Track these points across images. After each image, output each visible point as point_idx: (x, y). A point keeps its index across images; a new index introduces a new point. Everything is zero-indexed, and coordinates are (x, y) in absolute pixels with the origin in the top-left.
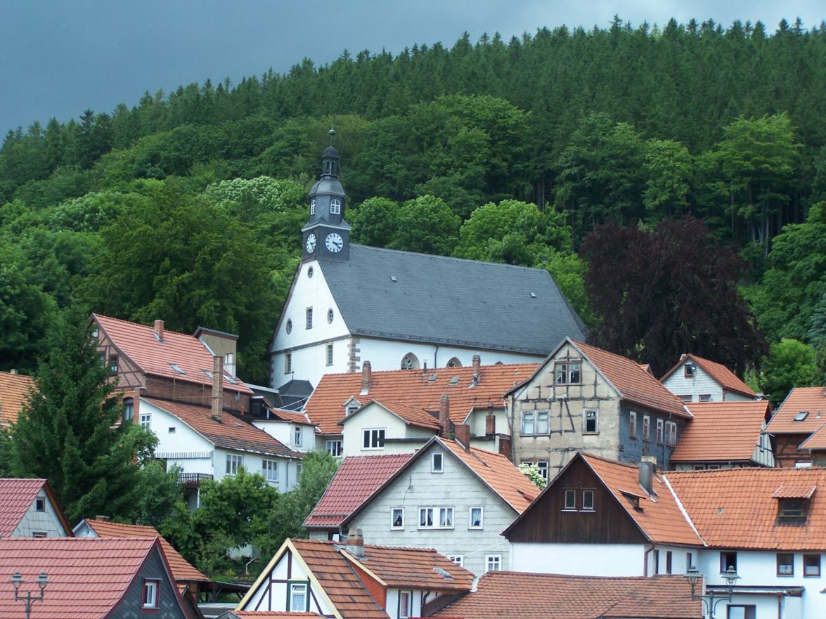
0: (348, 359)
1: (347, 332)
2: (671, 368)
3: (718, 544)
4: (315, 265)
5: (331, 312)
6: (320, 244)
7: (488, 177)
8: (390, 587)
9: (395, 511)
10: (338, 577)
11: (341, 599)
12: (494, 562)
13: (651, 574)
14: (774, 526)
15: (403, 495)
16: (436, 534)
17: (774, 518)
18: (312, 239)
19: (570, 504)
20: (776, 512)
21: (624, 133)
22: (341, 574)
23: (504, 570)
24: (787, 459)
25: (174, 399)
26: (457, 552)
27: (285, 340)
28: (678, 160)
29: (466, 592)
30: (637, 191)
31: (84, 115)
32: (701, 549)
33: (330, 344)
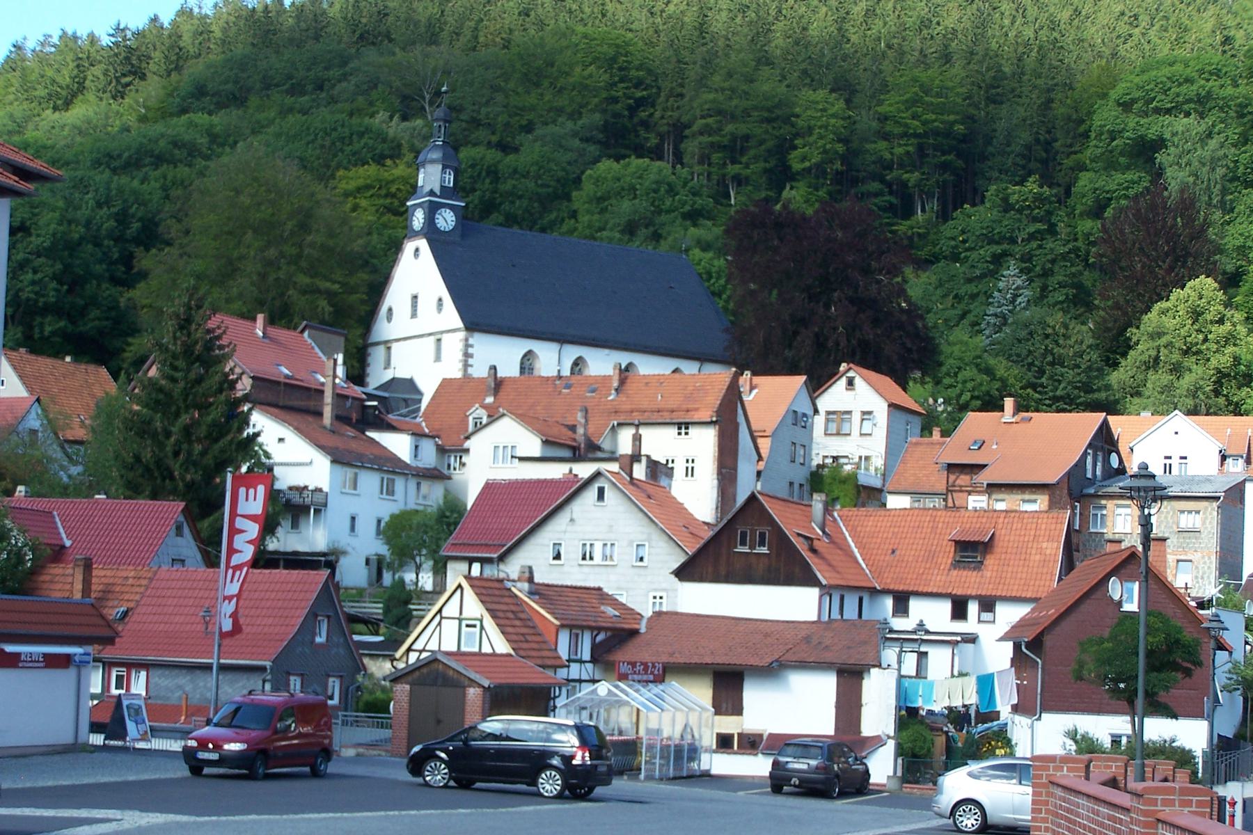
0: (460, 356)
1: (460, 324)
2: (827, 381)
3: (891, 587)
4: (423, 244)
5: (440, 300)
7: (606, 128)
8: (563, 626)
9: (554, 544)
10: (511, 615)
11: (515, 637)
12: (658, 600)
13: (825, 618)
14: (949, 570)
15: (563, 527)
16: (597, 570)
17: (949, 561)
19: (743, 543)
20: (952, 554)
22: (512, 612)
23: (670, 609)
24: (961, 491)
25: (281, 404)
26: (619, 588)
27: (384, 329)
29: (634, 633)
30: (784, 148)
31: (112, 32)
32: (874, 592)
33: (438, 336)
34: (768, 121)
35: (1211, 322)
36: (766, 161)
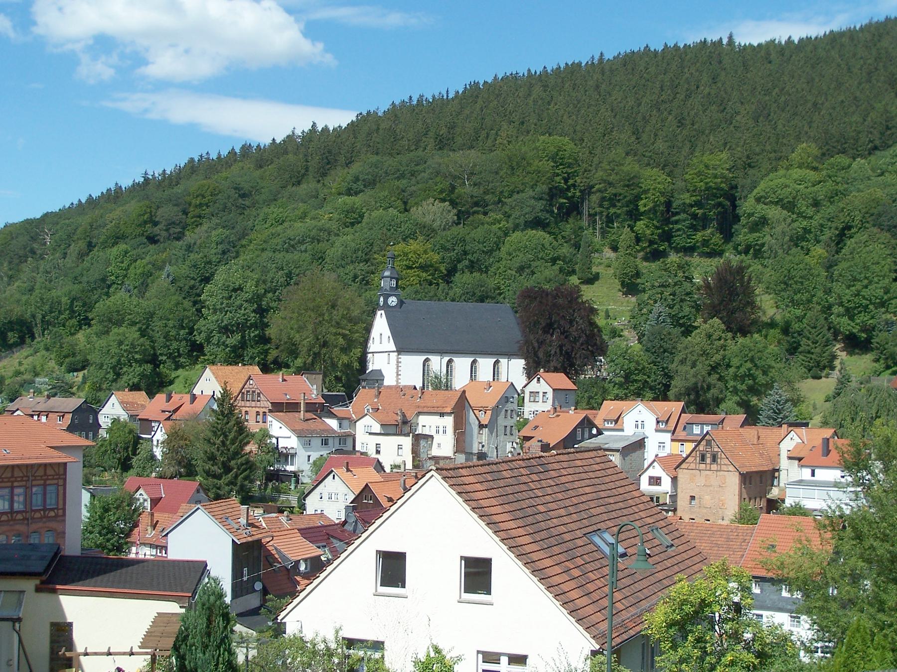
1: (395, 349)
4: (383, 312)
6: (385, 301)
18: (382, 299)
21: (630, 166)
28: (659, 183)
34: (628, 186)
35: (716, 340)
36: (627, 206)
